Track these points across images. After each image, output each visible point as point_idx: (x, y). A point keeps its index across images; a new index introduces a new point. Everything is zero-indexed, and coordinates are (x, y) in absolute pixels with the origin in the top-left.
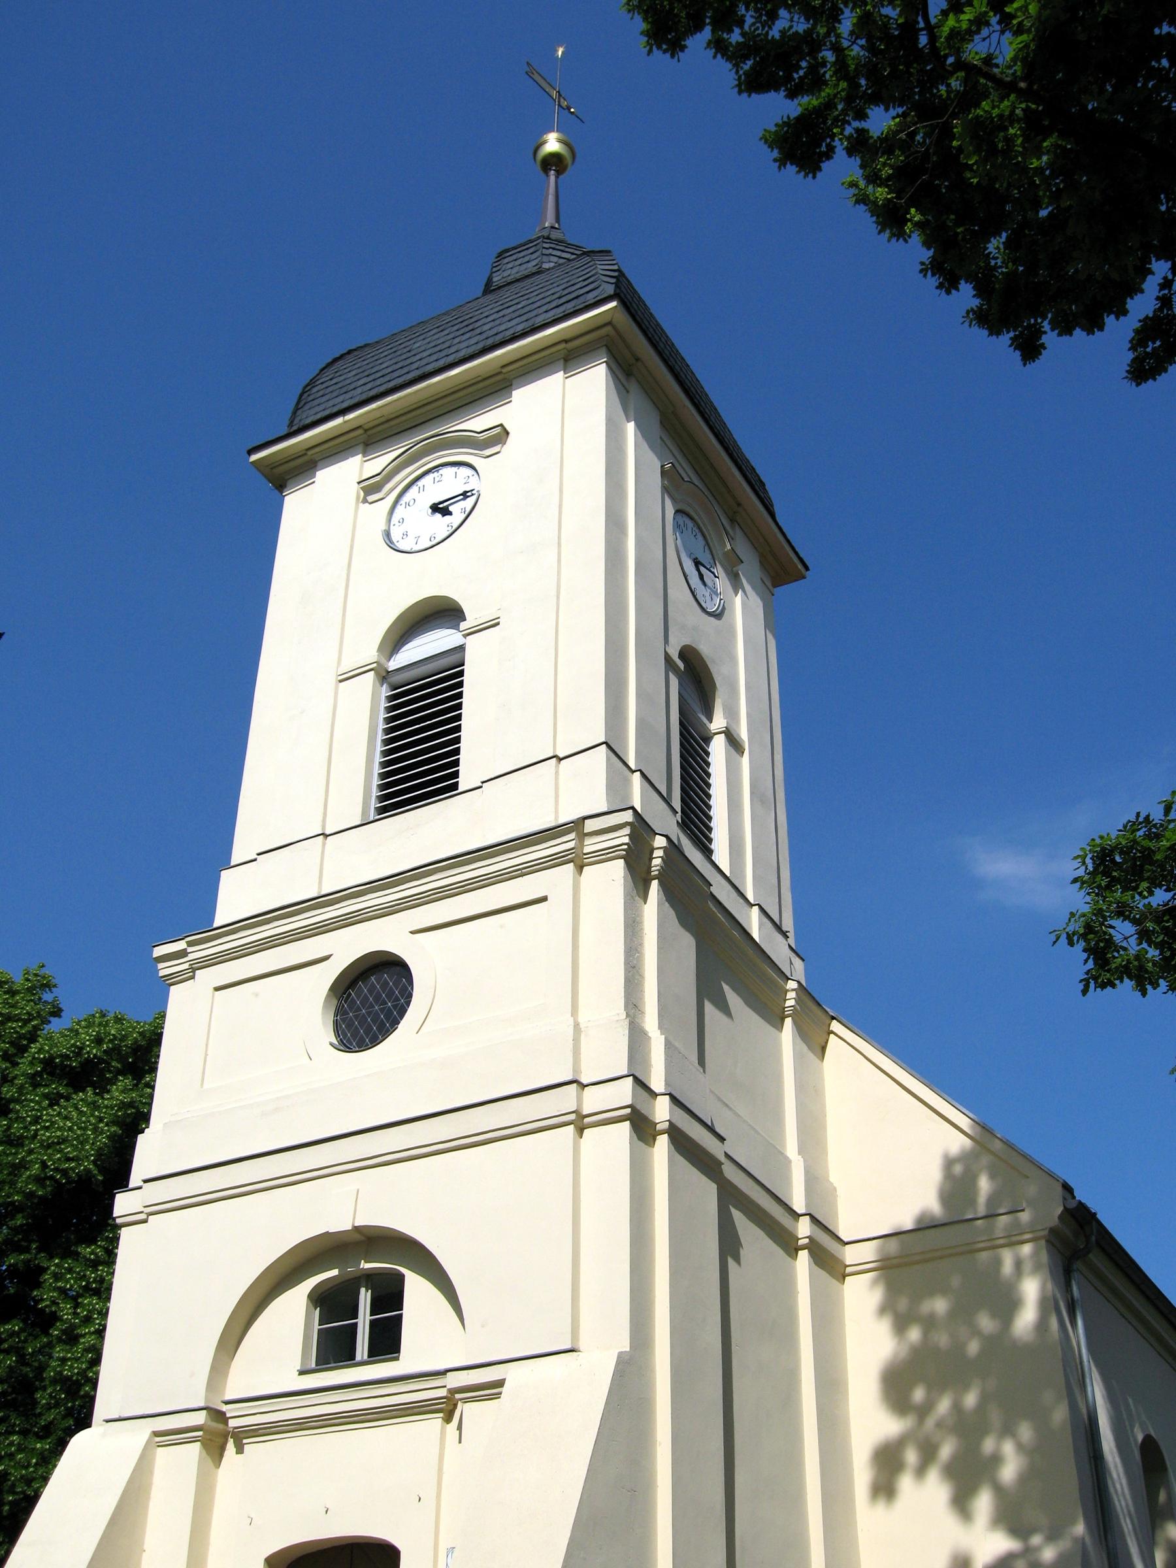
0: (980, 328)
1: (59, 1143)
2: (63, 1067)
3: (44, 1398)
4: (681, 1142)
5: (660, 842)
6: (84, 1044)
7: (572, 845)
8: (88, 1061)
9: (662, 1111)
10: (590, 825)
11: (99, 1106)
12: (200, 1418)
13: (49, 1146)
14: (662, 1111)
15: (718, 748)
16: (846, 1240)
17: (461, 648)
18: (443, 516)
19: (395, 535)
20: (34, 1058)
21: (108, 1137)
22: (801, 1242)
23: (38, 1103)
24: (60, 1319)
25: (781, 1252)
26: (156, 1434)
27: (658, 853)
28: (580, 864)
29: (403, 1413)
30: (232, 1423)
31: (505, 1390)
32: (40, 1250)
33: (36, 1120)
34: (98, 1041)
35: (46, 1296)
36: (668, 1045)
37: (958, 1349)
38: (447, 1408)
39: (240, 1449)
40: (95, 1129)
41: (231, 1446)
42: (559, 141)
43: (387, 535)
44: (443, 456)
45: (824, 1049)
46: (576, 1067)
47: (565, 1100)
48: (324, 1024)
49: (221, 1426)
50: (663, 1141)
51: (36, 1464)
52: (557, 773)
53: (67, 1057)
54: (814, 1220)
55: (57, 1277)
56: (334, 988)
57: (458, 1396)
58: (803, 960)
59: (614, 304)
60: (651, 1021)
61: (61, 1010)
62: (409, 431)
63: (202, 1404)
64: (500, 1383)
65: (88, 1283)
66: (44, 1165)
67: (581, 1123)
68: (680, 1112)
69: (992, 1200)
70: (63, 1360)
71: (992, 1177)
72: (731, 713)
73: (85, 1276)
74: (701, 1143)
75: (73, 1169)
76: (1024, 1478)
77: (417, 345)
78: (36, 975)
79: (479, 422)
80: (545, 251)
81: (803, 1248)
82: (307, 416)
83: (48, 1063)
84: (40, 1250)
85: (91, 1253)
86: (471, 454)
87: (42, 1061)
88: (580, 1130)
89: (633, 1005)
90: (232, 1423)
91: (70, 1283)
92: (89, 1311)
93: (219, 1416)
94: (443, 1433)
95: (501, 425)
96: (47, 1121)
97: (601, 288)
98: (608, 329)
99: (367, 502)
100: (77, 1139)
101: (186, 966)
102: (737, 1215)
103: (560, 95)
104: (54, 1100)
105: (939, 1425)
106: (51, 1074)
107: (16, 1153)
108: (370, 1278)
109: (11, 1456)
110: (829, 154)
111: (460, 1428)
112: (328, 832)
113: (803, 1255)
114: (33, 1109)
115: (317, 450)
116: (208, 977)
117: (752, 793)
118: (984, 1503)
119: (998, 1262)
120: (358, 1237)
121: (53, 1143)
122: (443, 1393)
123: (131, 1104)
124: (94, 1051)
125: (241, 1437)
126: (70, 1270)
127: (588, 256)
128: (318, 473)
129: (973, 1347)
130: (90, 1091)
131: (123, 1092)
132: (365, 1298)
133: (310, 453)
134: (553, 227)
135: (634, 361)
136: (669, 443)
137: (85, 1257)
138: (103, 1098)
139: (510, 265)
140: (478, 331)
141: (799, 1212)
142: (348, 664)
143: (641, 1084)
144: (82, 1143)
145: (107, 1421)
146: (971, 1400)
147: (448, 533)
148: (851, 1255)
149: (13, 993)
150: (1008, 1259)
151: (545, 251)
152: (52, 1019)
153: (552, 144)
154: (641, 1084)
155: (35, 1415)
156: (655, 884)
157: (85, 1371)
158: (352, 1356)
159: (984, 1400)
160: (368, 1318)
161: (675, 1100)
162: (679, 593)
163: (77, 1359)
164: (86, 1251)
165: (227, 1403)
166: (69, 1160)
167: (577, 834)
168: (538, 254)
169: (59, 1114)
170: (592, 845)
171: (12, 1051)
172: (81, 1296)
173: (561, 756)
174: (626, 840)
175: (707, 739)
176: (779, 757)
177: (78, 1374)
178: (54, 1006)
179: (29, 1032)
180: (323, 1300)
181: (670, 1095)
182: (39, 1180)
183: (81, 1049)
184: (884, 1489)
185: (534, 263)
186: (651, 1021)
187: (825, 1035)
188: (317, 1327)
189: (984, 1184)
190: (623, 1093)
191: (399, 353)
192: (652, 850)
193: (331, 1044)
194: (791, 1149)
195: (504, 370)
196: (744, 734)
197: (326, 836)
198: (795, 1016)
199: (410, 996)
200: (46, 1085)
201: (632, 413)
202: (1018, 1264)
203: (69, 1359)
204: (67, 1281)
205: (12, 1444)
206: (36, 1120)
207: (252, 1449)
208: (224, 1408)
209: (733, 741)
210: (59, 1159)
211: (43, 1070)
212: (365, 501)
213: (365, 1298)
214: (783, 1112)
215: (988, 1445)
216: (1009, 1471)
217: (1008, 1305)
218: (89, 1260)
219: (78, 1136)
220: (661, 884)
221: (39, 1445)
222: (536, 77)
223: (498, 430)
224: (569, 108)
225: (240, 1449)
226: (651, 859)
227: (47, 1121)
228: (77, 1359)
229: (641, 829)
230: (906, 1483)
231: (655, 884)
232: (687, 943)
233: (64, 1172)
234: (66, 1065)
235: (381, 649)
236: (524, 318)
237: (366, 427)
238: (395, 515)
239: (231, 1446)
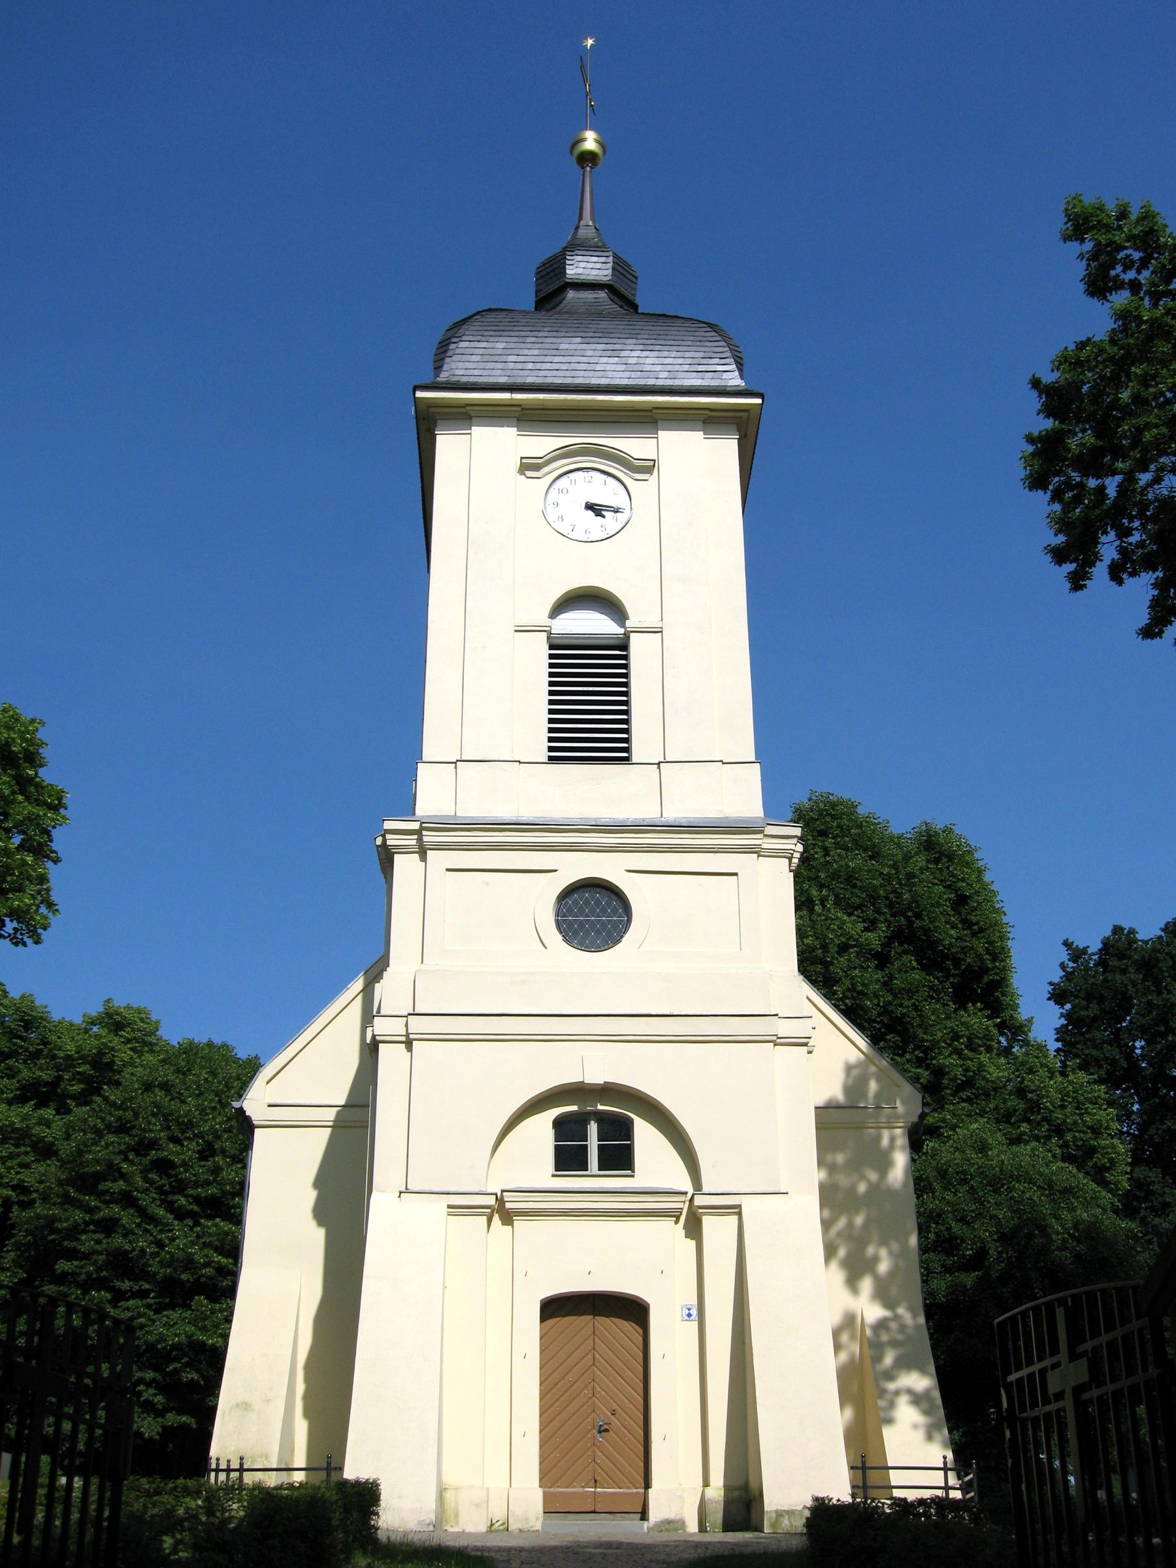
18: (596, 515)
19: (552, 515)
26: (449, 1207)
29: (644, 1214)
37: (852, 1189)
42: (596, 141)
44: (601, 463)
62: (553, 423)
69: (878, 1095)
71: (878, 1080)
76: (892, 1274)
79: (634, 446)
86: (622, 471)
99: (525, 475)
105: (839, 1234)
108: (601, 1118)
118: (867, 1285)
119: (879, 1137)
127: (715, 331)
129: (862, 1188)
132: (593, 1128)
146: (859, 1220)
150: (886, 1135)
153: (590, 142)
180: (560, 1124)
188: (588, 1143)
189: (873, 1086)
195: (655, 411)
202: (892, 1139)
213: (593, 1128)
215: (870, 1250)
216: (883, 1267)
217: (884, 1163)
237: (524, 407)
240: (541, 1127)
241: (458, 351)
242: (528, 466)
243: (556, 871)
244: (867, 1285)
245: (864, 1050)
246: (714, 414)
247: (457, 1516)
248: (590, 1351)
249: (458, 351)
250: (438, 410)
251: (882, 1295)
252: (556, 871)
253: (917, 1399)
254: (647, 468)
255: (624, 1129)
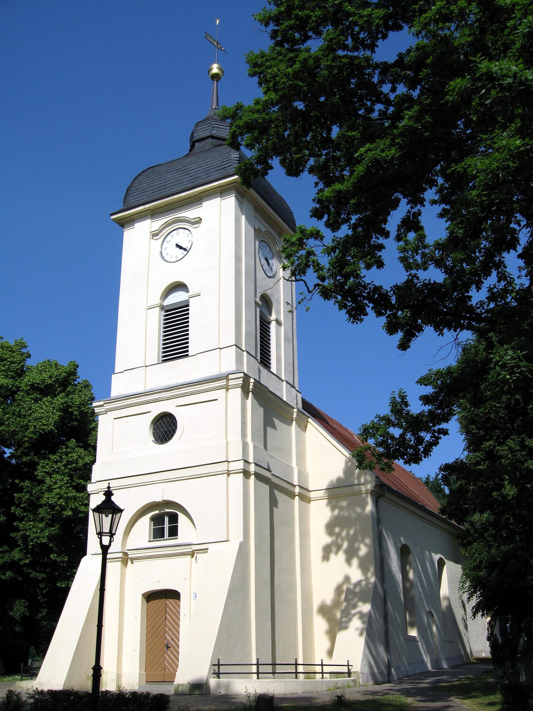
0: (330, 300)
1: (40, 419)
2: (37, 387)
3: (42, 511)
4: (258, 476)
5: (252, 380)
6: (45, 378)
7: (225, 383)
8: (47, 385)
9: (252, 468)
10: (231, 377)
11: (53, 403)
12: (120, 555)
13: (36, 420)
14: (252, 468)
15: (273, 326)
16: (311, 490)
17: (188, 301)
20: (26, 384)
21: (58, 416)
22: (296, 494)
23: (30, 401)
24: (46, 483)
25: (290, 498)
27: (252, 384)
28: (227, 388)
30: (130, 556)
31: (208, 551)
32: (34, 455)
33: (30, 409)
34: (51, 377)
35: (39, 473)
36: (254, 446)
38: (192, 554)
39: (132, 563)
40: (53, 413)
41: (129, 561)
42: (218, 68)
43: (161, 253)
45: (306, 427)
46: (227, 457)
47: (223, 467)
48: (150, 434)
49: (126, 557)
50: (253, 477)
51: (40, 532)
52: (220, 354)
53: (39, 384)
54: (300, 487)
55: (43, 467)
56: (152, 422)
57: (195, 552)
58: (301, 393)
59: (236, 177)
60: (249, 439)
61: (30, 355)
63: (120, 550)
64: (207, 549)
65: (54, 469)
66: (35, 427)
67: (228, 473)
68: (258, 467)
70: (48, 498)
72: (278, 312)
73: (53, 466)
74: (264, 475)
75: (46, 429)
76: (367, 555)
77: (169, 177)
78: (20, 343)
79: (191, 214)
80: (213, 126)
81: (297, 495)
82: (132, 201)
83: (32, 386)
84: (34, 455)
85: (55, 458)
87: (29, 385)
88: (228, 475)
89: (244, 435)
90: (130, 556)
91: (48, 469)
92: (56, 480)
93: (126, 554)
94: (191, 560)
95: (199, 217)
96: (34, 409)
97: (233, 166)
98: (236, 184)
100: (46, 417)
101: (104, 410)
102: (276, 491)
103: (218, 43)
104: (36, 400)
106: (34, 390)
107: (24, 421)
109: (30, 529)
110: (302, 171)
111: (196, 559)
112: (147, 365)
113: (297, 498)
114: (28, 404)
115: (134, 216)
116: (112, 414)
117: (285, 340)
118: (355, 562)
120: (164, 502)
121: (38, 418)
122: (191, 550)
123: (65, 403)
124: (49, 381)
125: (132, 560)
126: (47, 464)
128: (135, 224)
130: (49, 397)
131: (62, 398)
132: (166, 519)
133: (132, 217)
134: (216, 109)
135: (244, 192)
136: (258, 217)
137: (52, 460)
138: (54, 399)
139: (200, 130)
140: (190, 175)
141: (296, 484)
142: (151, 303)
143: (246, 462)
144: (48, 418)
145: (92, 555)
146: (352, 532)
147: (183, 256)
148: (312, 495)
149: (13, 352)
151: (213, 126)
152: (27, 359)
153: (215, 69)
154: (246, 462)
155: (37, 514)
156: (251, 393)
157: (56, 501)
158: (163, 536)
159: (356, 531)
160: (168, 525)
161: (256, 464)
162: (260, 274)
163: (53, 498)
164: (53, 457)
165: (128, 550)
166: (44, 425)
167: (227, 380)
168: (211, 127)
169: (38, 406)
170: (231, 383)
171: (15, 375)
172: (52, 474)
173: (221, 347)
174: (241, 382)
175: (269, 323)
176: (295, 321)
177: (54, 503)
178: (28, 354)
179: (20, 367)
181: (255, 463)
182: (34, 433)
183: (44, 380)
184: (326, 557)
185: (209, 131)
186: (249, 439)
187: (306, 423)
188: (152, 527)
190: (240, 465)
191: (162, 179)
192: (250, 383)
193: (153, 441)
194: (294, 465)
195: (200, 195)
196: (282, 319)
197: (146, 366)
198: (296, 420)
199: (176, 426)
200: (32, 394)
201: (244, 212)
203: (50, 497)
204: (47, 468)
205: (30, 525)
206: (30, 409)
207: (136, 563)
208: (127, 551)
209: (278, 323)
210: (41, 425)
211: (30, 388)
212: (153, 239)
213: (166, 519)
214: (292, 451)
215: (356, 545)
217: (364, 505)
218: (54, 461)
219: (47, 416)
220: (253, 393)
221: (40, 526)
222: (209, 38)
223: (198, 219)
224: (221, 48)
225: (132, 563)
226: (249, 386)
227: (34, 409)
228: (53, 498)
229: (246, 378)
230: (332, 556)
231: (251, 393)
232: (261, 410)
233: (43, 430)
234: (39, 387)
235: (161, 298)
236: (206, 173)
238: (163, 245)
239: (129, 561)
240: (145, 522)
241: (131, 192)
242: (155, 235)
243: (150, 412)
244: (355, 562)
245: (348, 456)
246: (222, 188)
247: (106, 684)
248: (164, 615)
249: (131, 192)
250: (123, 221)
251: (363, 567)
252: (150, 412)
253: (362, 616)
254: (199, 221)
255: (174, 518)
